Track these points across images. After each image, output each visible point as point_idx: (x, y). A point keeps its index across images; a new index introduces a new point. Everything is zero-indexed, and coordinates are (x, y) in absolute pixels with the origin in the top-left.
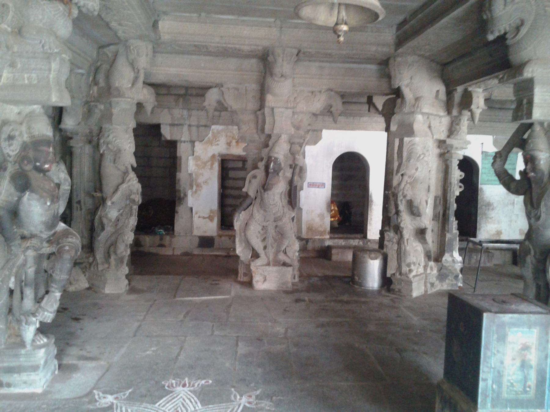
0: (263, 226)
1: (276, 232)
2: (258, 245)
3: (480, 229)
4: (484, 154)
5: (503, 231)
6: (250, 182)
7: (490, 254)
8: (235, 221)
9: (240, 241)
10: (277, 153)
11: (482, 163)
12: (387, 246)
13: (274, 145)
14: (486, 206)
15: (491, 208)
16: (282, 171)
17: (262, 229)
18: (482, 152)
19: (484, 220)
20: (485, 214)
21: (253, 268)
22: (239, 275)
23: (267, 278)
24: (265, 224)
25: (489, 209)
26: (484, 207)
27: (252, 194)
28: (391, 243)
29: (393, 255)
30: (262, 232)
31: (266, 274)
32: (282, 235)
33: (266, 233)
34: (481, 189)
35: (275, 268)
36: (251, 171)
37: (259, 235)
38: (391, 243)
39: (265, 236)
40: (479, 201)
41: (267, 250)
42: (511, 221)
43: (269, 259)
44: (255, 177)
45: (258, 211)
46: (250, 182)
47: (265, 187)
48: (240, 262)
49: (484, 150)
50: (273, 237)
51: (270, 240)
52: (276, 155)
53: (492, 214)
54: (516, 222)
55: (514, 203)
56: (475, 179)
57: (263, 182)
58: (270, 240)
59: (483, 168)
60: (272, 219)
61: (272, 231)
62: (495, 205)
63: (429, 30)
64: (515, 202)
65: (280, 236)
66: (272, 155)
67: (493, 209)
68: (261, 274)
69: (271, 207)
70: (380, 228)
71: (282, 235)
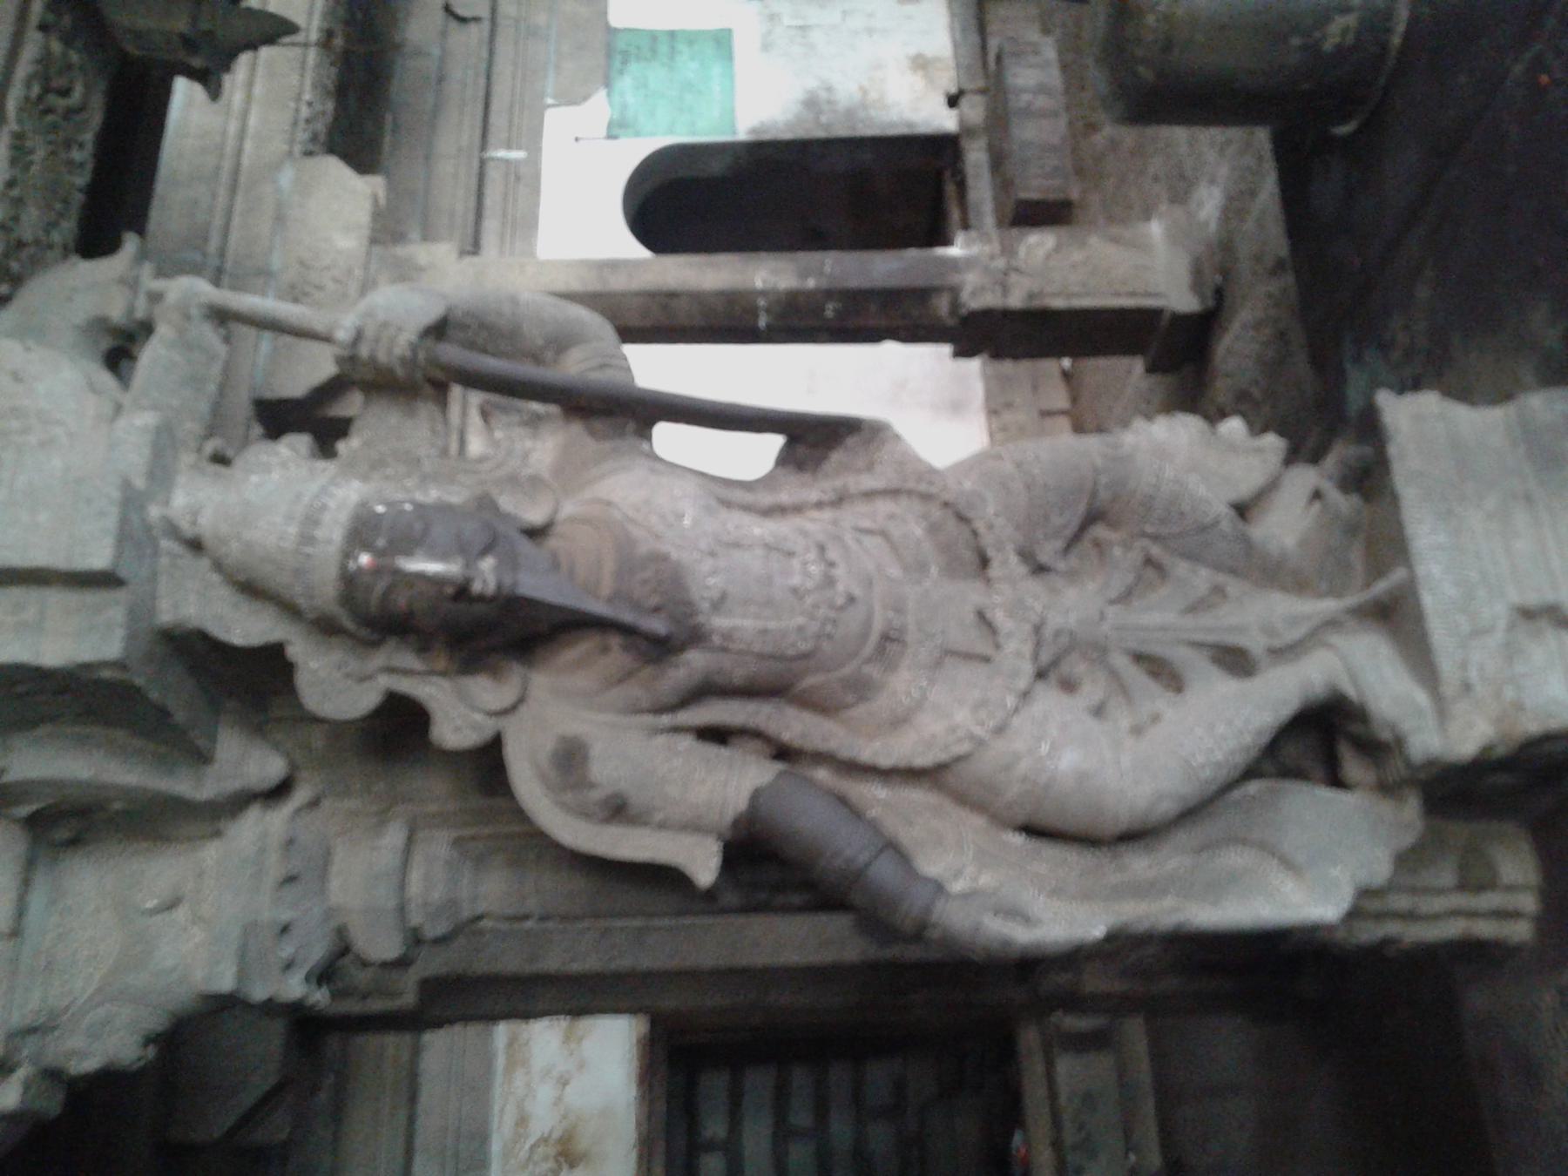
0: (1041, 675)
1: (1072, 576)
2: (1222, 720)
3: (910, 125)
4: (615, 131)
5: (912, 51)
6: (618, 811)
7: (1007, 48)
8: (1022, 936)
9: (1216, 889)
10: (312, 520)
11: (653, 134)
12: (1031, 296)
13: (251, 589)
14: (820, 112)
15: (823, 95)
16: (506, 502)
17: (1069, 686)
18: (611, 136)
19: (873, 113)
20: (850, 113)
21: (1464, 736)
22: (1485, 929)
23: (1533, 599)
24: (1017, 651)
25: (829, 102)
26: (824, 119)
27: (732, 783)
28: (1014, 278)
29: (1074, 266)
30: (1093, 690)
31: (1497, 612)
32: (1094, 517)
33: (1097, 652)
34: (753, 131)
35: (1425, 532)
36: (520, 814)
37: (1123, 719)
38: (1014, 278)
39: (1121, 662)
40: (800, 133)
41: (1255, 643)
42: (870, 31)
43: (1332, 624)
44: (570, 760)
45: (899, 721)
46: (618, 811)
47: (651, 637)
48: (1369, 933)
49: (604, 132)
50: (1125, 597)
51: (1159, 617)
52: (333, 532)
53: (847, 90)
54: (871, 15)
55: (803, 28)
56: (716, 167)
57: (617, 656)
58: (1159, 617)
59: (671, 132)
60: (972, 594)
61: (1075, 603)
62: (812, 84)
63: (747, 1153)
64: (800, 22)
65: (1099, 531)
66: (325, 591)
67: (829, 89)
68: (1510, 652)
69: (845, 582)
70: (946, 349)
71: (1094, 517)
